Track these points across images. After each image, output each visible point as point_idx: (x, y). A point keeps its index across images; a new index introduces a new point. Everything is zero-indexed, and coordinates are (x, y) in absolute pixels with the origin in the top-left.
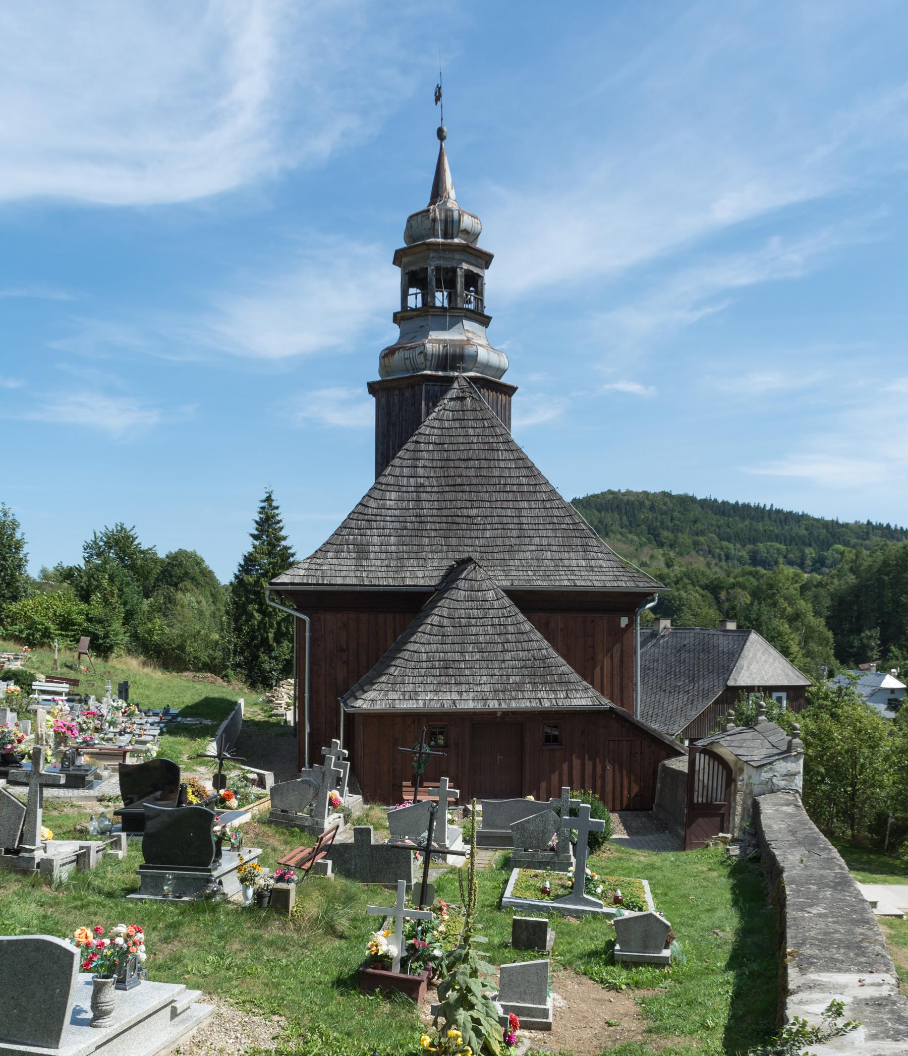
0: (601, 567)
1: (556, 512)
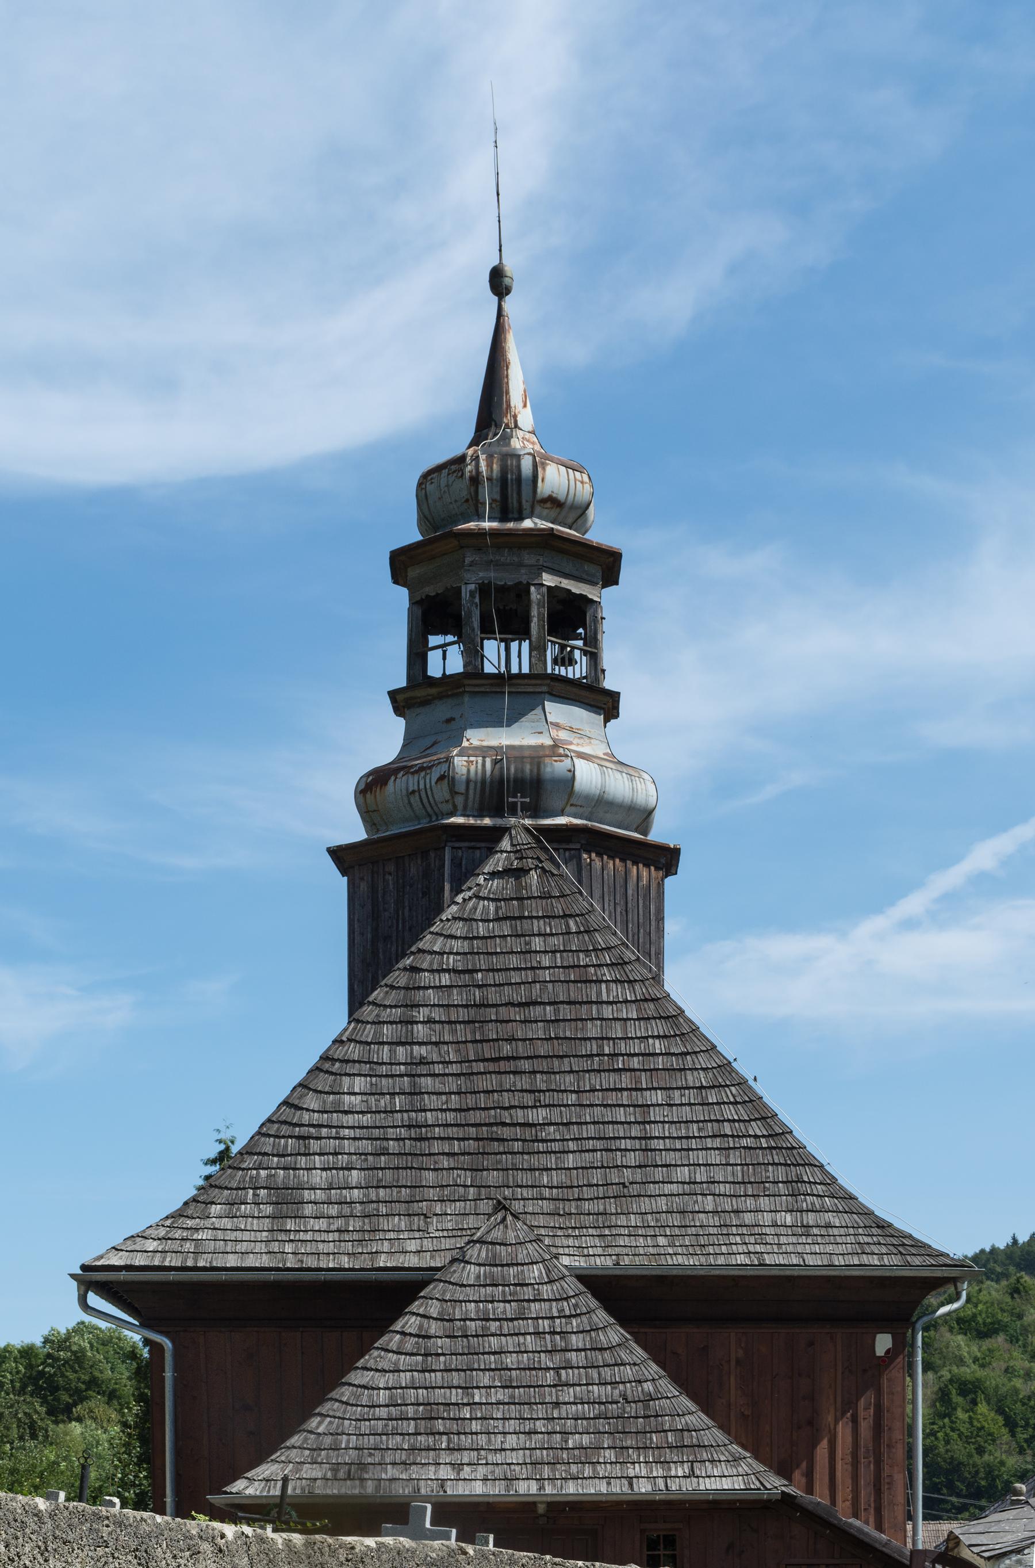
0: (828, 1226)
1: (729, 1112)
